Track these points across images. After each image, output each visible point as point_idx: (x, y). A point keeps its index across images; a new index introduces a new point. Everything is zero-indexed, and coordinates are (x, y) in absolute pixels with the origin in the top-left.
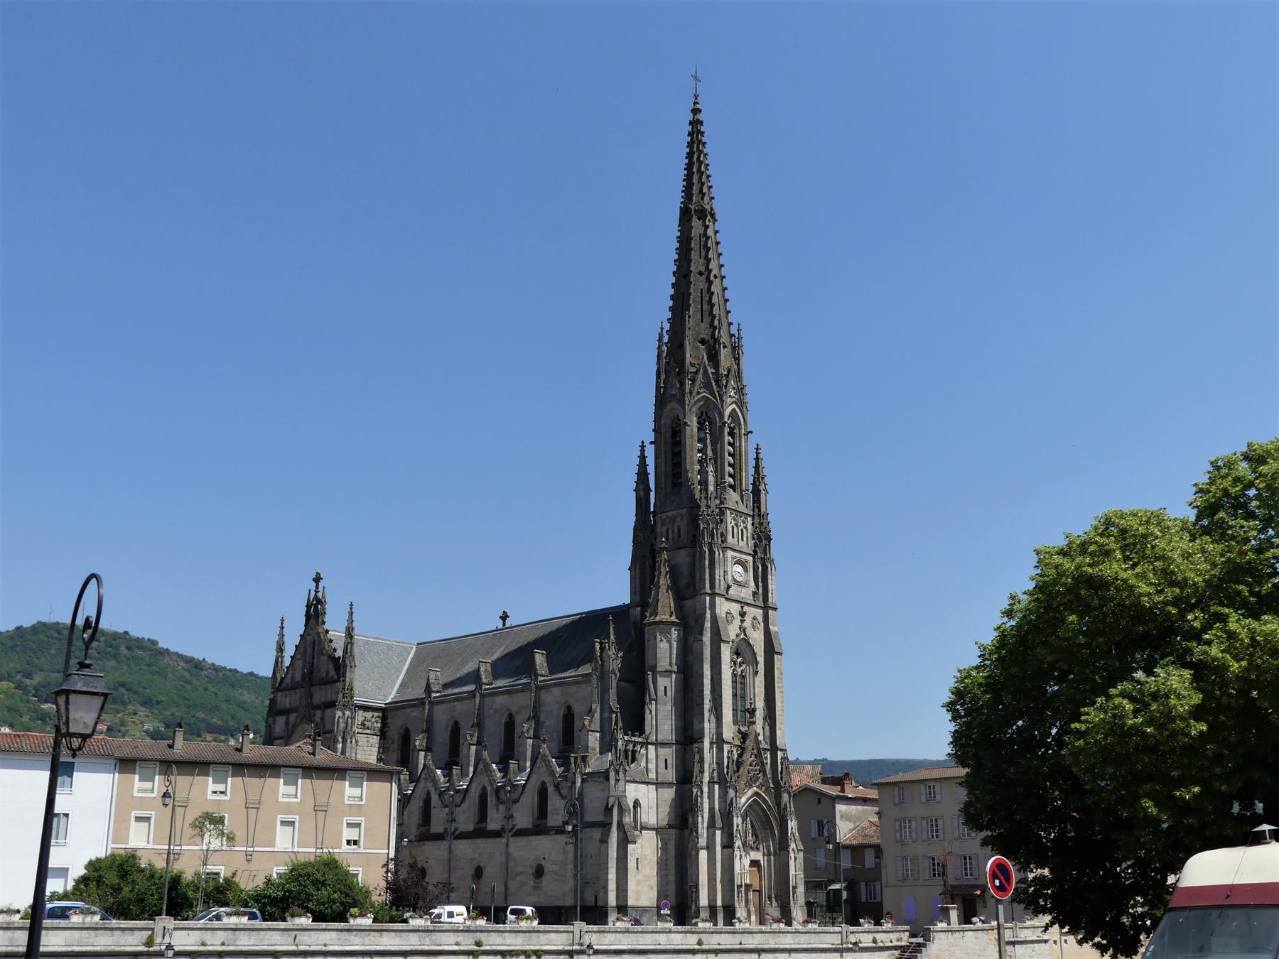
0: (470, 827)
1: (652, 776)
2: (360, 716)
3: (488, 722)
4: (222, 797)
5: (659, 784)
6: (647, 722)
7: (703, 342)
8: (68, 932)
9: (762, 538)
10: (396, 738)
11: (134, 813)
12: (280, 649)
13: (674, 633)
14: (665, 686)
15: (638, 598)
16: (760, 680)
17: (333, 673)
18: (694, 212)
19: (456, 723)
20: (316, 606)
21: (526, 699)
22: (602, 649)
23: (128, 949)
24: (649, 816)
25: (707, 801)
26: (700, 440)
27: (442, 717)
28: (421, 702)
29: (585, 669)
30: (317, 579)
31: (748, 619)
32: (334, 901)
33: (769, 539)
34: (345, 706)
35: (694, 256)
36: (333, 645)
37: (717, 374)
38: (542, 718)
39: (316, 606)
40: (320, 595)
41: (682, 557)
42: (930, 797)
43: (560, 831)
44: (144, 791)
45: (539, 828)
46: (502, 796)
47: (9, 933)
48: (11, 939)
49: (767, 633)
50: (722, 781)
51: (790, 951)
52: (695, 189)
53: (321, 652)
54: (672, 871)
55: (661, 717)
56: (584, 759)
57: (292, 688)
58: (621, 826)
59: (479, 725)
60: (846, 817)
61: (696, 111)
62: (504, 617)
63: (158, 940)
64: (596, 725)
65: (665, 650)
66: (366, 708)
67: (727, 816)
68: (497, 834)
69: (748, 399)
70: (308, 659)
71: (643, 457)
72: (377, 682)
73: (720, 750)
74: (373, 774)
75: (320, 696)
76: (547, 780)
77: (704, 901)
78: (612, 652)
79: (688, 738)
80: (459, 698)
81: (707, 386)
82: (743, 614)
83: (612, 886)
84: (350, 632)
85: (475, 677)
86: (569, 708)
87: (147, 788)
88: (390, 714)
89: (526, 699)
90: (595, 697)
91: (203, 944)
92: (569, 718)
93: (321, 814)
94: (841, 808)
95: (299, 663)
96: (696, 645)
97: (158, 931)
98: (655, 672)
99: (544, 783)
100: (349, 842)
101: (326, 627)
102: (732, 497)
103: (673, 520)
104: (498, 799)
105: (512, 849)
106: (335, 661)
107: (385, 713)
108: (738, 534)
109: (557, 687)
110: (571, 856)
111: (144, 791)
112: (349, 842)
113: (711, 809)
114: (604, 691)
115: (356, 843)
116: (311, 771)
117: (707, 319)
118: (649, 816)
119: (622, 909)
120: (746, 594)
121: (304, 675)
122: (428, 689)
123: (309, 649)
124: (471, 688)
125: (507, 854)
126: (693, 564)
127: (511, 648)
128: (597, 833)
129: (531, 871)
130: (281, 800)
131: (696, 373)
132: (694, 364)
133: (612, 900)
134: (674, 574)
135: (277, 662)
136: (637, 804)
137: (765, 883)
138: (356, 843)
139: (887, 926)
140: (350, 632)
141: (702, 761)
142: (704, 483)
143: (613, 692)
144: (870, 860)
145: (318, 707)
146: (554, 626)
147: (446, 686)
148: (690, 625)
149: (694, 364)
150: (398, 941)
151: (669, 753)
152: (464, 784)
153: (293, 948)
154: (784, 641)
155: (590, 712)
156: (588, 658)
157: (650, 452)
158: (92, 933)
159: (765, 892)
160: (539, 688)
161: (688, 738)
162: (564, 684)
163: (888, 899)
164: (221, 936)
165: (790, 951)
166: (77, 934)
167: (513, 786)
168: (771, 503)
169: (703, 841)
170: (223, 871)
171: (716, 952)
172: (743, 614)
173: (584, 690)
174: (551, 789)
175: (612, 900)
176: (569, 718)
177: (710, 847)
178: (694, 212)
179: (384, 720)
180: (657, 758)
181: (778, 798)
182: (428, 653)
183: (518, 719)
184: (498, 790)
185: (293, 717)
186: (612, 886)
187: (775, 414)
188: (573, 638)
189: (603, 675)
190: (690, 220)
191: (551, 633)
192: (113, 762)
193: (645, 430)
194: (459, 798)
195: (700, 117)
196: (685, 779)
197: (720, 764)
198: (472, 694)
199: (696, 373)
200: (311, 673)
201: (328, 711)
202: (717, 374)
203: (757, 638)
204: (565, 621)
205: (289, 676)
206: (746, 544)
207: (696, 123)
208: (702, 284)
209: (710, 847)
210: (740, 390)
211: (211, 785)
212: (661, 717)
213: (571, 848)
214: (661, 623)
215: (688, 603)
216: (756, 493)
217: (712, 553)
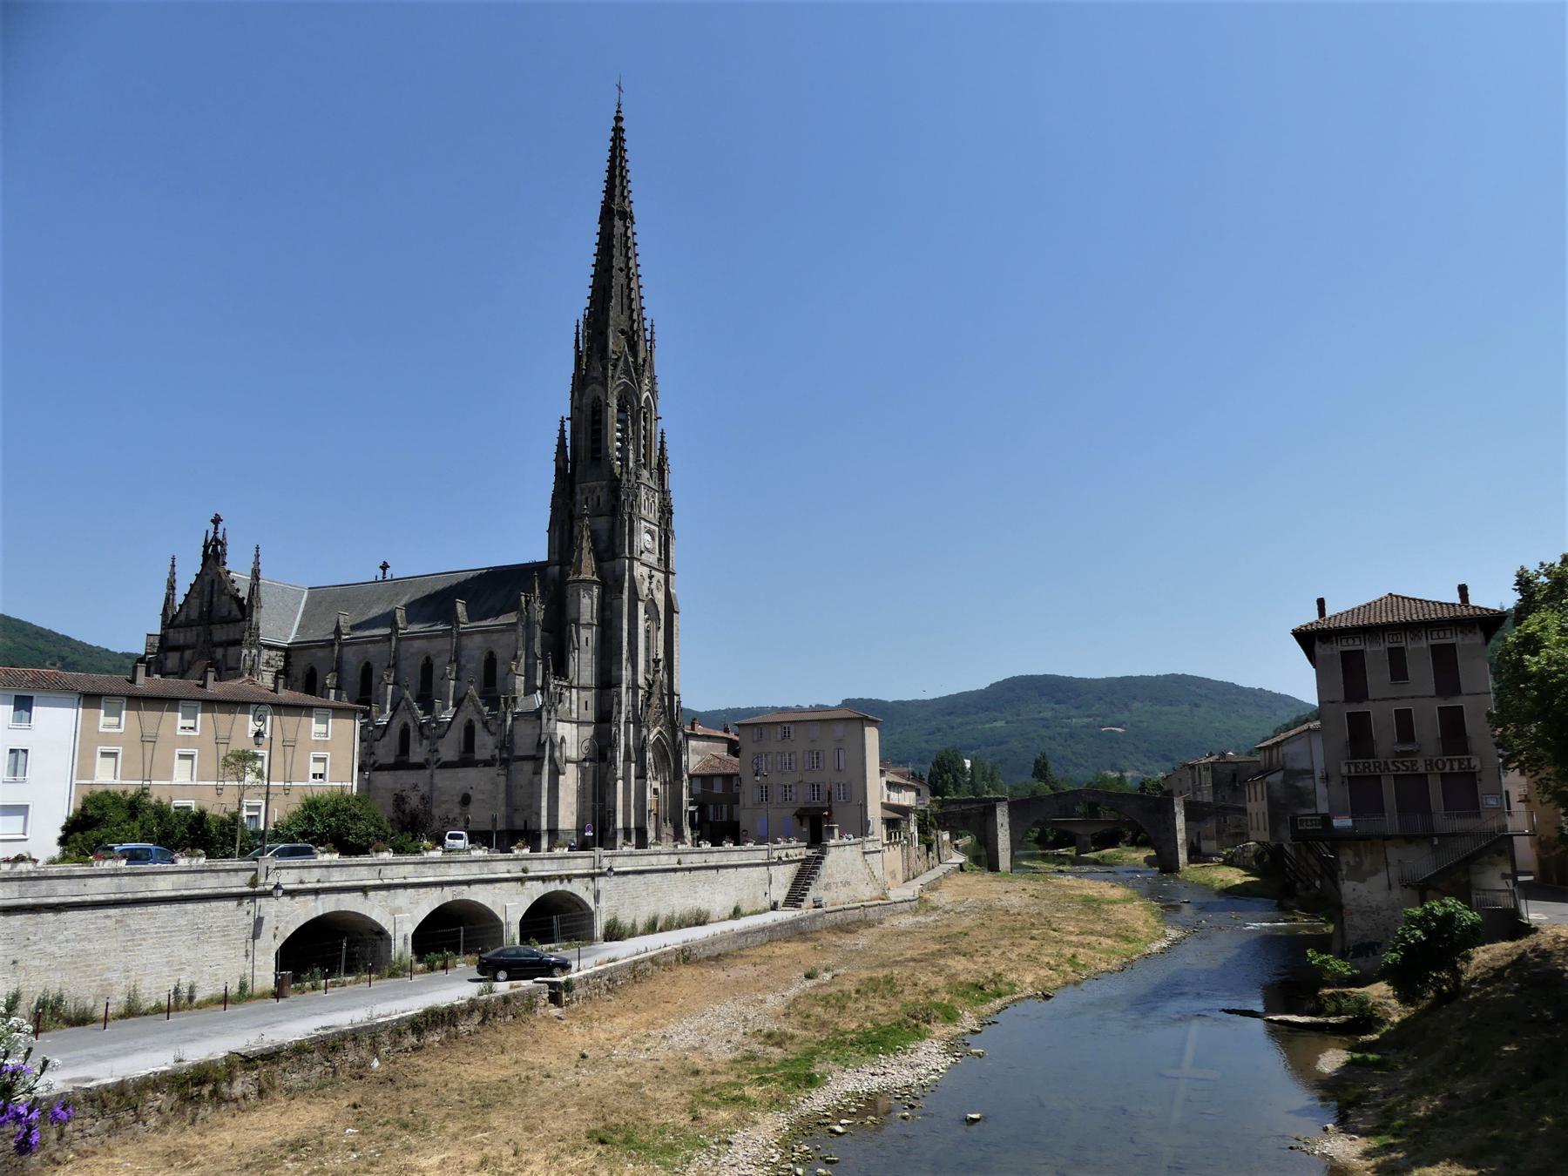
0: (391, 760)
1: (574, 715)
2: (265, 654)
3: (405, 665)
4: (192, 733)
5: (579, 723)
6: (571, 669)
7: (622, 332)
8: (175, 877)
9: (666, 511)
10: (300, 676)
11: (100, 749)
12: (171, 587)
13: (596, 591)
14: (587, 635)
15: (556, 557)
16: (661, 634)
17: (236, 612)
18: (615, 211)
19: (368, 664)
20: (215, 548)
21: (445, 644)
22: (527, 602)
23: (235, 890)
24: (572, 751)
25: (624, 737)
26: (619, 421)
27: (352, 658)
28: (330, 643)
29: (511, 618)
30: (216, 521)
31: (654, 581)
32: (369, 835)
33: (671, 513)
34: (251, 645)
35: (616, 252)
36: (236, 586)
37: (635, 362)
38: (463, 662)
39: (215, 548)
40: (220, 536)
41: (602, 523)
42: (786, 735)
43: (488, 763)
44: (110, 726)
45: (467, 759)
46: (426, 732)
47: (116, 880)
48: (119, 886)
49: (668, 595)
50: (637, 721)
51: (736, 866)
52: (617, 192)
53: (222, 592)
54: (590, 798)
55: (583, 665)
56: (514, 699)
57: (189, 624)
58: (552, 759)
59: (395, 666)
60: (696, 751)
61: (618, 119)
62: (385, 567)
63: (262, 880)
64: (521, 670)
65: (587, 605)
66: (270, 647)
67: (641, 751)
68: (420, 766)
69: (658, 388)
70: (206, 599)
71: (562, 431)
72: (280, 625)
73: (635, 694)
74: (338, 712)
75: (220, 633)
76: (475, 717)
77: (620, 824)
78: (537, 605)
79: (606, 683)
80: (372, 641)
81: (627, 372)
82: (651, 577)
83: (544, 813)
84: (256, 574)
85: (388, 619)
86: (491, 653)
87: (113, 723)
88: (293, 654)
89: (445, 644)
90: (520, 644)
91: (302, 882)
92: (491, 662)
93: (149, 746)
94: (692, 743)
95: (195, 603)
96: (615, 602)
97: (262, 871)
98: (578, 625)
99: (470, 721)
100: (314, 776)
101: (227, 567)
102: (645, 473)
103: (592, 491)
104: (422, 734)
105: (437, 779)
106: (240, 601)
107: (288, 652)
108: (648, 507)
109: (477, 631)
110: (502, 786)
111: (110, 726)
112: (314, 776)
113: (627, 745)
114: (529, 639)
115: (321, 776)
116: (210, 704)
117: (626, 312)
118: (572, 751)
119: (553, 832)
120: (652, 559)
121: (201, 612)
122: (338, 631)
123: (207, 589)
124: (387, 631)
125: (432, 785)
126: (612, 529)
127: (418, 596)
128: (528, 767)
129: (457, 799)
130: (101, 730)
131: (618, 359)
132: (610, 348)
133: (544, 826)
134: (594, 539)
135: (167, 599)
136: (563, 739)
137: (661, 808)
138: (321, 776)
139: (794, 843)
140: (256, 574)
141: (620, 703)
142: (624, 460)
143: (537, 640)
144: (718, 788)
145: (220, 644)
146: (462, 577)
147: (354, 628)
148: (611, 584)
149: (610, 348)
150: (462, 871)
151: (589, 696)
152: (383, 720)
153: (379, 882)
154: (680, 603)
155: (515, 657)
156: (515, 607)
157: (568, 425)
158: (198, 876)
159: (661, 815)
160: (460, 635)
161: (606, 683)
162: (488, 632)
163: (745, 818)
164: (317, 873)
165: (736, 866)
166: (184, 877)
167: (438, 723)
168: (672, 481)
169: (620, 773)
170: (193, 805)
171: (690, 870)
172: (651, 577)
173: (509, 638)
174: (478, 726)
175: (544, 826)
176: (491, 662)
177: (626, 779)
178: (615, 211)
179: (287, 658)
180: (579, 702)
181: (674, 735)
182: (321, 598)
183: (437, 662)
184: (421, 727)
185: (188, 654)
186: (544, 813)
187: (683, 401)
188: (494, 588)
189: (529, 626)
190: (612, 220)
191: (459, 584)
192: (76, 697)
193: (561, 405)
194: (378, 734)
195: (623, 124)
196: (604, 718)
197: (634, 706)
198: (388, 638)
199: (618, 359)
200: (210, 612)
201: (232, 650)
202: (635, 362)
203: (660, 597)
204: (472, 574)
205: (183, 615)
206: (654, 516)
207: (618, 130)
208: (623, 281)
209: (626, 779)
210: (653, 379)
211: (180, 720)
212: (583, 665)
213: (503, 779)
214: (584, 581)
215: (606, 565)
216: (661, 470)
217: (631, 519)
